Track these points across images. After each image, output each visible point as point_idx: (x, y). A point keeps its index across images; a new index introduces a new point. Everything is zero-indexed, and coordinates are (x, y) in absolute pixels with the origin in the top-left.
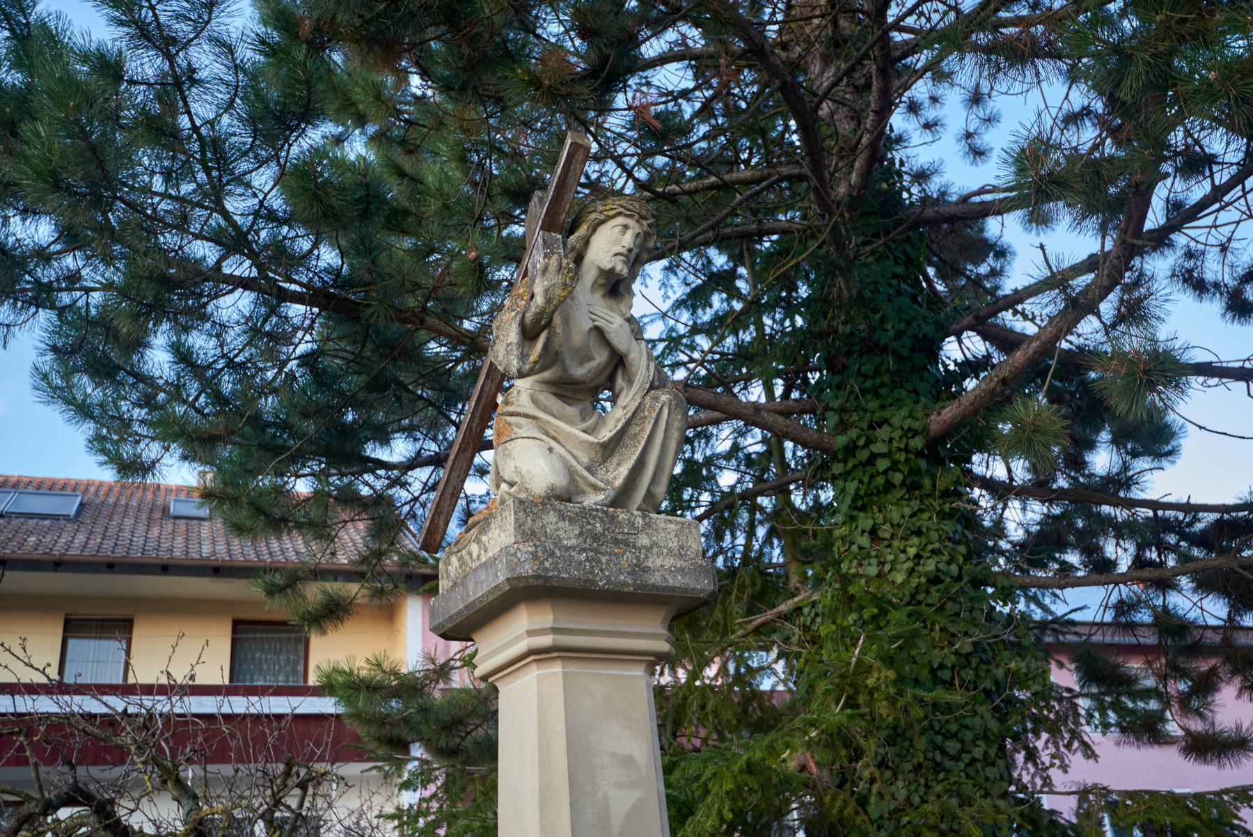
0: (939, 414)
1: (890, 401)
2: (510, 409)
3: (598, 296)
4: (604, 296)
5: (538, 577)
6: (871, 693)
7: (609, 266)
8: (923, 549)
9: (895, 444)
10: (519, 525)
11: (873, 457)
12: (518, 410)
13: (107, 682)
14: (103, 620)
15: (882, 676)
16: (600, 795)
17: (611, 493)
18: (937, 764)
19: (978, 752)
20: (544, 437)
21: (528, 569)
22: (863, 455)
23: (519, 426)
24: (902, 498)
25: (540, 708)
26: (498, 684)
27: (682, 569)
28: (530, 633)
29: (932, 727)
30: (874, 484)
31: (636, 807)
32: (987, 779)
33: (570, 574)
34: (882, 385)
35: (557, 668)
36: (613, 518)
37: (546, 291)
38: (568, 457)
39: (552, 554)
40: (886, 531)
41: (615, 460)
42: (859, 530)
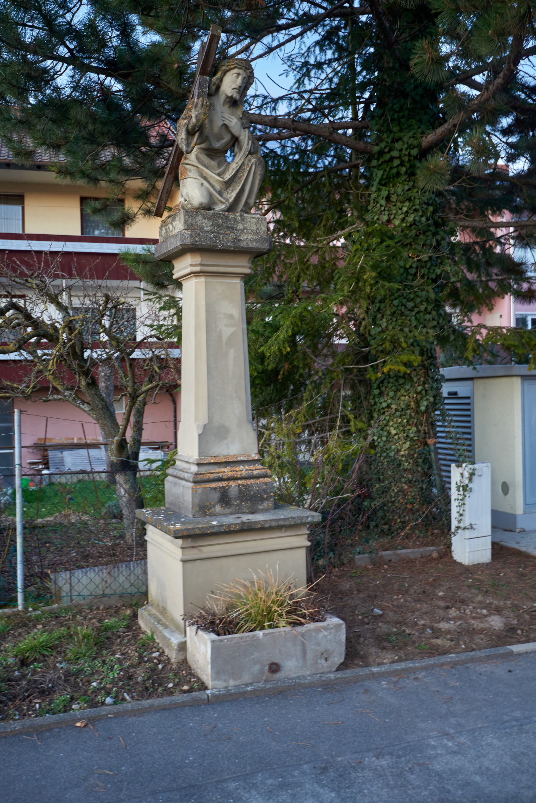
0: (426, 137)
1: (406, 126)
2: (187, 162)
3: (226, 107)
4: (229, 107)
5: (193, 244)
6: (365, 282)
7: (230, 95)
8: (410, 209)
9: (404, 152)
10: (186, 222)
11: (392, 159)
12: (190, 162)
13: (14, 241)
14: (7, 195)
15: (369, 275)
16: (218, 329)
17: (228, 205)
18: (403, 313)
19: (422, 308)
20: (200, 178)
21: (188, 241)
22: (387, 157)
23: (190, 171)
24: (405, 180)
25: (196, 294)
26: (183, 282)
27: (256, 240)
28: (191, 265)
29: (403, 295)
30: (391, 173)
31: (233, 334)
32: (425, 320)
33: (206, 243)
34: (403, 117)
35: (202, 279)
36: (227, 217)
37: (196, 116)
38: (210, 188)
39: (199, 235)
40: (394, 198)
41: (231, 188)
42: (381, 197)
